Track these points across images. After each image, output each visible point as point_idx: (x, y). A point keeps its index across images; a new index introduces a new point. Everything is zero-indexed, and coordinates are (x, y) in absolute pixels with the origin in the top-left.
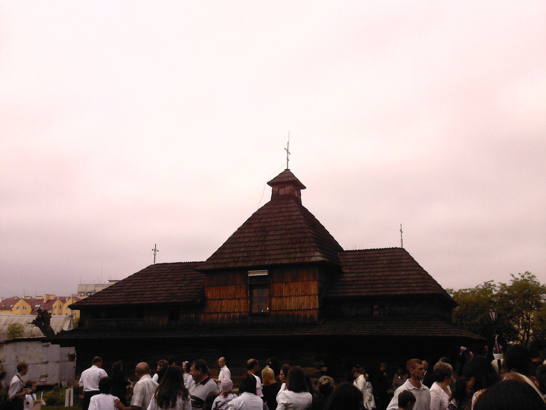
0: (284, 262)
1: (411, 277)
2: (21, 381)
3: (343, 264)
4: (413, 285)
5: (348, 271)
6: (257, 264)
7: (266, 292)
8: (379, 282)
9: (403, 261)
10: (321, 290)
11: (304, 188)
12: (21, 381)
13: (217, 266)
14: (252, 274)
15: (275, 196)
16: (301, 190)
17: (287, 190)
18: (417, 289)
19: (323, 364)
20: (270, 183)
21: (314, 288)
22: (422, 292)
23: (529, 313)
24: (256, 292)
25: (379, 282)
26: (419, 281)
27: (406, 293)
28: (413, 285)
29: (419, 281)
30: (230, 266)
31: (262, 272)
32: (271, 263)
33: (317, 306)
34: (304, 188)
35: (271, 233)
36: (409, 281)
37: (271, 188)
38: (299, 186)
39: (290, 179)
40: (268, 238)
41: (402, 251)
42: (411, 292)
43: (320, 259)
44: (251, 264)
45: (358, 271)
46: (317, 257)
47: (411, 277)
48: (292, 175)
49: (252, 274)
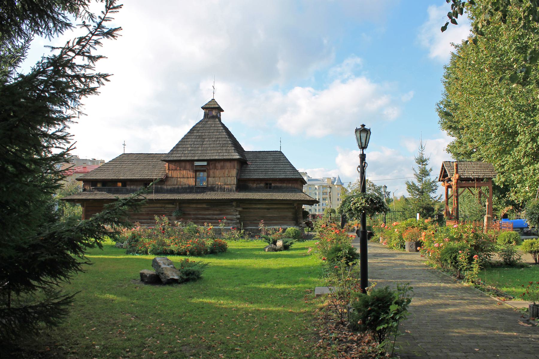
0: (217, 157)
1: (287, 168)
2: (403, 254)
3: (248, 159)
4: (288, 173)
5: (250, 163)
6: (201, 158)
7: (206, 174)
8: (269, 170)
9: (281, 159)
10: (237, 174)
11: (223, 111)
12: (403, 254)
14: (196, 163)
15: (206, 115)
16: (221, 113)
17: (214, 113)
18: (290, 175)
19: (238, 214)
20: (203, 108)
21: (234, 172)
22: (293, 177)
23: (50, 82)
24: (198, 173)
25: (269, 170)
26: (291, 171)
27: (284, 177)
28: (288, 173)
29: (291, 171)
30: (182, 158)
32: (208, 158)
33: (236, 184)
34: (223, 111)
35: (207, 140)
36: (286, 171)
38: (220, 110)
39: (217, 106)
40: (205, 143)
41: (280, 152)
42: (287, 177)
43: (238, 157)
44: (196, 158)
45: (256, 164)
46: (237, 156)
47: (287, 168)
49: (196, 163)
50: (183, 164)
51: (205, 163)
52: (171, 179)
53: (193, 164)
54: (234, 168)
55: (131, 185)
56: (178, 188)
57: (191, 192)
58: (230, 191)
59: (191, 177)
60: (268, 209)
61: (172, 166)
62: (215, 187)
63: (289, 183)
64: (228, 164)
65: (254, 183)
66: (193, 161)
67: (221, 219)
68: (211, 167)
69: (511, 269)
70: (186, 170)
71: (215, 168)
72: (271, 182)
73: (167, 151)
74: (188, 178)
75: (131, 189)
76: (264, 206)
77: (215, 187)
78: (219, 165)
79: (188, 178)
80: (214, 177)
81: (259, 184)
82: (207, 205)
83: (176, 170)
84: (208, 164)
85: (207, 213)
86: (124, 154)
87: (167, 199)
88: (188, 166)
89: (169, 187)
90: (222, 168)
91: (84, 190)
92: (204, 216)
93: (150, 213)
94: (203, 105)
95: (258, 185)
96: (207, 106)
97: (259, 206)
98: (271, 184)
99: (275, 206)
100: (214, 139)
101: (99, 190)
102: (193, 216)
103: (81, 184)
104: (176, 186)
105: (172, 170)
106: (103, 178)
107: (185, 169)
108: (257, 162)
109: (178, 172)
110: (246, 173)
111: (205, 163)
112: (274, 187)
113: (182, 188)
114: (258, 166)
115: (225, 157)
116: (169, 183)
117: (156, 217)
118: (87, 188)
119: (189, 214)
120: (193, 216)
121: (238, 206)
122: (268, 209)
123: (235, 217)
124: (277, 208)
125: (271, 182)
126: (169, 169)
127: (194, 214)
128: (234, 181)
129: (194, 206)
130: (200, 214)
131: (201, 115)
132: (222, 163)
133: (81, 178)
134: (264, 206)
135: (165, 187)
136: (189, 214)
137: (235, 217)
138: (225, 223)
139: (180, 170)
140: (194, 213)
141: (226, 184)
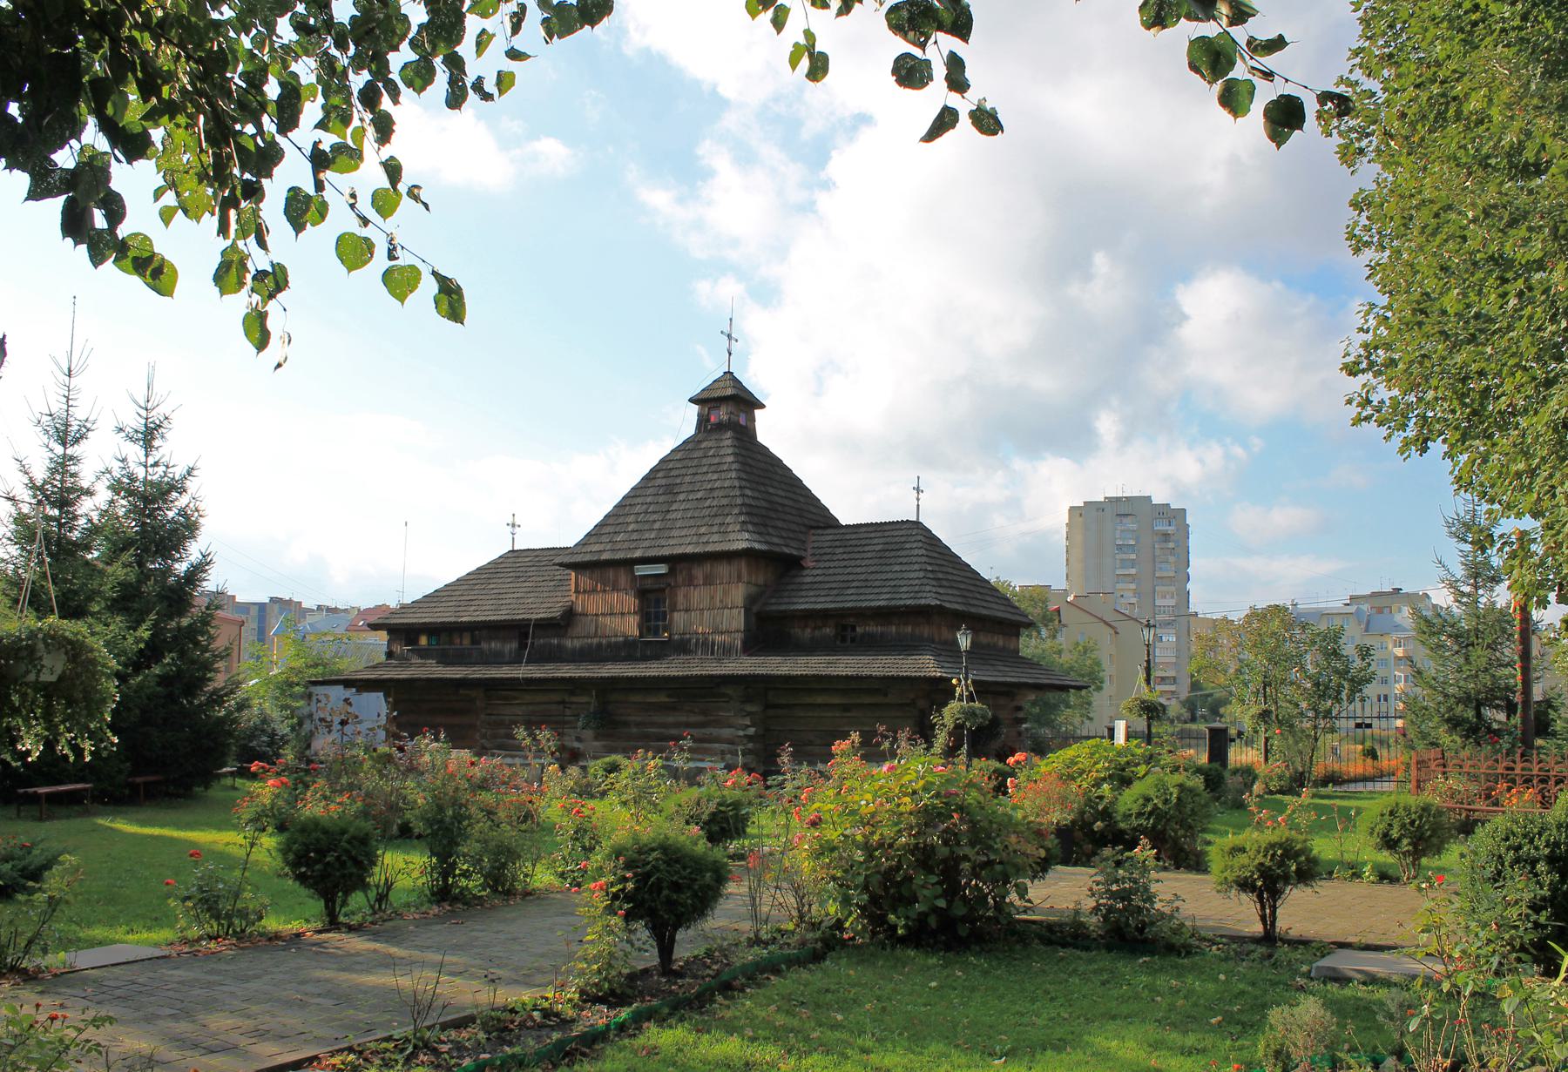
0: (689, 550)
11: (762, 406)
13: (618, 556)
14: (641, 570)
15: (702, 422)
16: (757, 413)
20: (691, 400)
30: (604, 557)
31: (652, 569)
34: (762, 406)
35: (682, 497)
37: (695, 408)
41: (917, 524)
44: (638, 554)
48: (737, 383)
49: (641, 570)
50: (611, 573)
51: (662, 569)
52: (583, 618)
53: (633, 572)
54: (739, 578)
55: (490, 639)
56: (599, 645)
57: (615, 659)
58: (727, 651)
59: (629, 613)
60: (846, 708)
61: (585, 581)
62: (690, 640)
63: (906, 624)
64: (723, 570)
65: (806, 626)
66: (630, 563)
67: (677, 739)
68: (680, 579)
69: (970, 970)
70: (618, 590)
71: (690, 582)
72: (851, 621)
73: (571, 544)
74: (623, 614)
75: (490, 650)
76: (836, 700)
77: (690, 640)
78: (699, 572)
79: (623, 614)
80: (687, 610)
81: (819, 628)
82: (669, 696)
83: (594, 591)
84: (672, 571)
85: (671, 719)
86: (513, 551)
87: (563, 679)
88: (623, 580)
89: (577, 643)
90: (709, 581)
91: (390, 655)
92: (662, 730)
93: (533, 718)
94: (695, 390)
95: (817, 633)
96: (706, 396)
97: (820, 700)
98: (854, 628)
99: (867, 700)
100: (699, 495)
101: (423, 654)
102: (634, 730)
103: (382, 638)
104: (595, 641)
105: (585, 592)
106: (427, 620)
107: (615, 589)
108: (835, 558)
109: (599, 598)
110: (786, 594)
111: (662, 569)
112: (863, 635)
113: (609, 645)
114: (831, 571)
115: (710, 548)
116: (578, 630)
117: (521, 733)
118: (397, 648)
119: (626, 724)
120: (634, 730)
121: (748, 699)
122: (846, 708)
123: (741, 733)
124: (826, 705)
125: (851, 621)
126: (577, 592)
127: (638, 725)
128: (735, 620)
129: (637, 698)
130: (653, 724)
131: (686, 422)
132: (707, 567)
133: (380, 621)
134: (836, 700)
135: (569, 643)
136: (626, 724)
137: (741, 733)
138: (691, 750)
139: (605, 591)
140: (639, 719)
141: (717, 631)
